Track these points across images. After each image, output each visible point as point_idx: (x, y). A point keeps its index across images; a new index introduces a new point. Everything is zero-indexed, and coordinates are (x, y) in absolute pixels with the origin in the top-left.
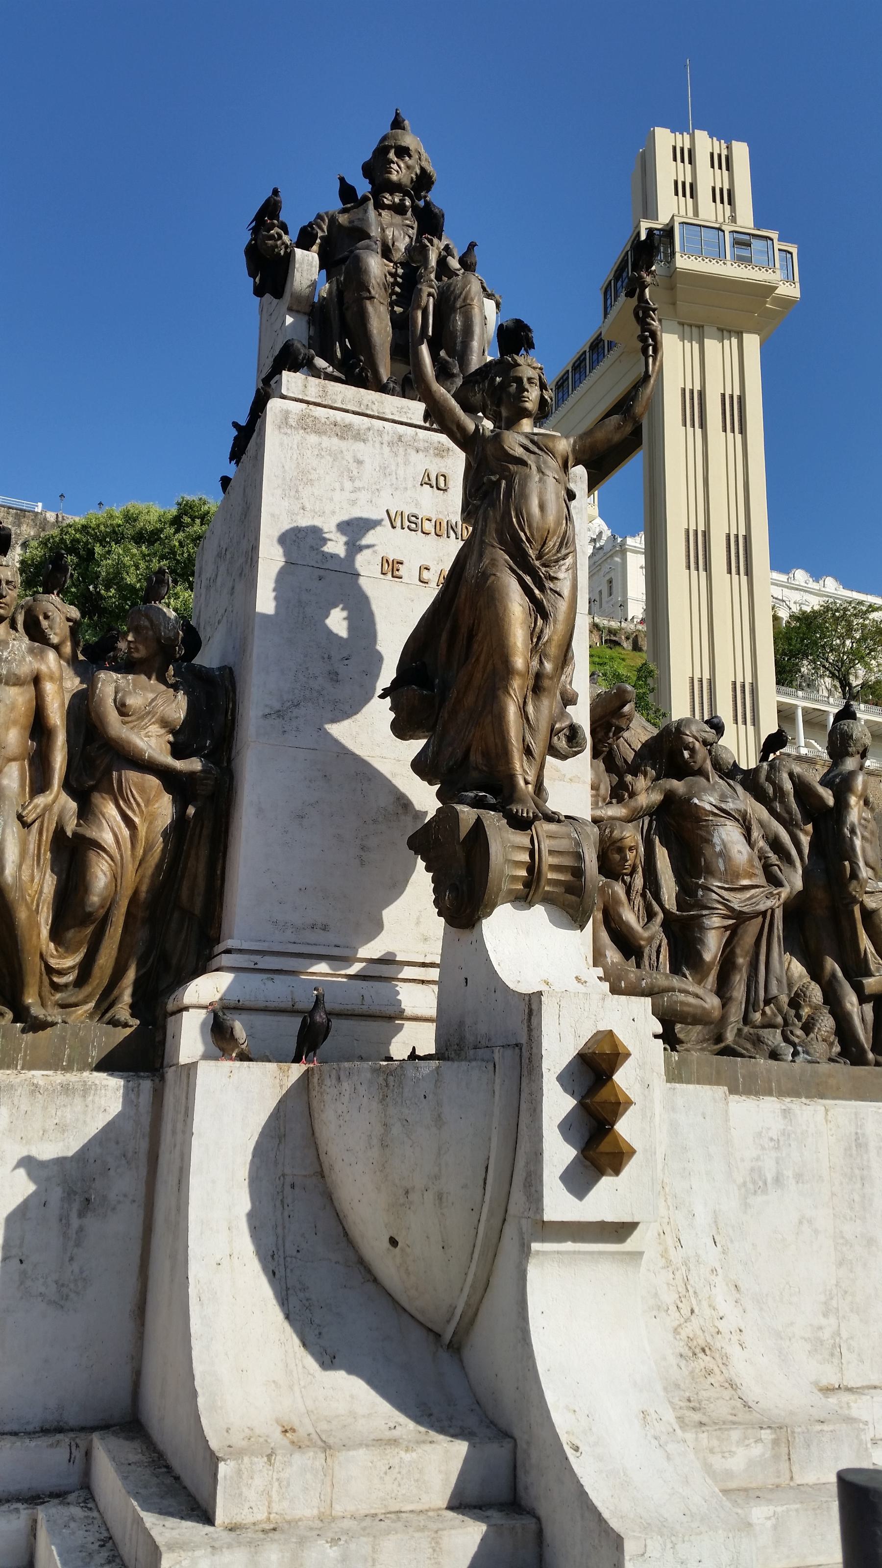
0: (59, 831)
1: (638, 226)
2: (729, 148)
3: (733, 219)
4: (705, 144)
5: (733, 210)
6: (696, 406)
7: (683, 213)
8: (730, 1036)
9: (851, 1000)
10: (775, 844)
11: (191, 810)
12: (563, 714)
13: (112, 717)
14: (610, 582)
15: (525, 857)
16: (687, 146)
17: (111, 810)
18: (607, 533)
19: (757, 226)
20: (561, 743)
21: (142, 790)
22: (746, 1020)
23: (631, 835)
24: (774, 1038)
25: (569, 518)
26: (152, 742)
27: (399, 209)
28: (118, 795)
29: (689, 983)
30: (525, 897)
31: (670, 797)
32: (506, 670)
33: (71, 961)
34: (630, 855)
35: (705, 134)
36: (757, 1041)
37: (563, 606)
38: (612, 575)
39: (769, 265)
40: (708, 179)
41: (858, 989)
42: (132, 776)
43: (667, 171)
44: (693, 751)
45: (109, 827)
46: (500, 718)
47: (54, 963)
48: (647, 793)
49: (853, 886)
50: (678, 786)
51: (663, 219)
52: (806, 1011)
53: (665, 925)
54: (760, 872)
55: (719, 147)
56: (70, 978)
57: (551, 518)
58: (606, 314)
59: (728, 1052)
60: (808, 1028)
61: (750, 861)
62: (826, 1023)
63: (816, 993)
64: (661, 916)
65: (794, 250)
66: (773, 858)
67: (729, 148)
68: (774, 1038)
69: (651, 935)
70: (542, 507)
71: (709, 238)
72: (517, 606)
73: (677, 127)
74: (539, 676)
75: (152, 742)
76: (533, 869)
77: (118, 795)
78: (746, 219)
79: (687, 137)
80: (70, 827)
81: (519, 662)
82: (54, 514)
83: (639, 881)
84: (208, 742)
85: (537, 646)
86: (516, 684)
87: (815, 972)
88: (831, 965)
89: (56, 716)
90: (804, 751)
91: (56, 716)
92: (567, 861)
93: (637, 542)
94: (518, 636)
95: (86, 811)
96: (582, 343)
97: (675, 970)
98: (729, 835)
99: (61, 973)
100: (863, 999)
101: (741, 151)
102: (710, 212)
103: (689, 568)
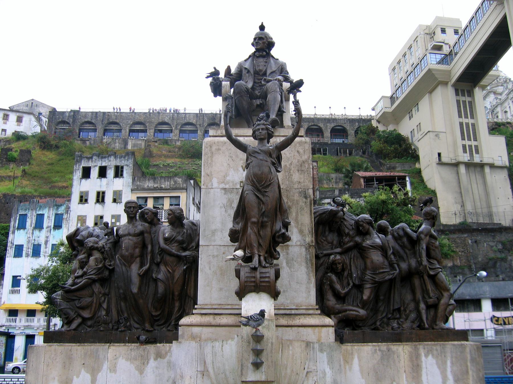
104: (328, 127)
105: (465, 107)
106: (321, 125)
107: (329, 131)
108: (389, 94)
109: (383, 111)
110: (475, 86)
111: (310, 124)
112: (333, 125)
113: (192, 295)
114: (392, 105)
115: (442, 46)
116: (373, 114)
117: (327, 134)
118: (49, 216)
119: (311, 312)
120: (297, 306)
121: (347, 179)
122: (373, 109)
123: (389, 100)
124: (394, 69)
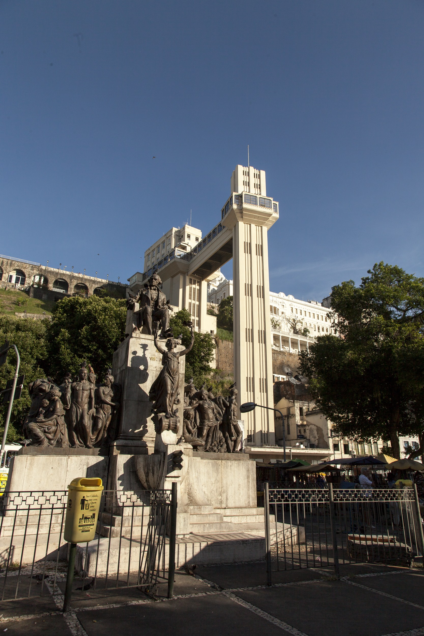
0: (93, 415)
1: (232, 194)
2: (260, 172)
3: (260, 194)
4: (252, 170)
5: (260, 191)
6: (248, 247)
7: (245, 191)
8: (208, 448)
9: (230, 442)
10: (219, 413)
11: (115, 412)
12: (177, 398)
13: (102, 395)
14: (224, 294)
15: (168, 423)
16: (247, 171)
17: (102, 412)
18: (224, 278)
19: (267, 196)
20: (176, 402)
21: (107, 408)
22: (211, 445)
23: (192, 413)
24: (215, 448)
25: (178, 368)
26: (108, 400)
27: (155, 290)
28: (103, 409)
29: (200, 439)
30: (168, 430)
31: (200, 404)
32: (167, 393)
33: (95, 437)
34: (191, 416)
35: (253, 168)
36: (212, 449)
37: (176, 383)
38: (225, 292)
39: (270, 207)
40: (253, 181)
41: (231, 439)
42: (106, 405)
43: (241, 178)
44: (204, 396)
45: (102, 415)
46: (166, 400)
47: (92, 438)
48: (196, 403)
49: (231, 421)
50: (201, 402)
51: (240, 192)
52: (222, 443)
53: (197, 428)
54: (214, 418)
55: (257, 172)
56: (94, 440)
57: (175, 367)
58: (222, 218)
59: (207, 451)
60: (221, 446)
61: (213, 417)
62: (225, 446)
63: (224, 440)
64: (196, 427)
65: (277, 203)
66: (218, 415)
67: (260, 172)
68: (215, 448)
69: (195, 430)
70: (174, 367)
71: (253, 200)
72: (169, 382)
73: (245, 165)
74: (172, 393)
75: (108, 400)
76: (169, 425)
77: (103, 409)
78: (264, 193)
79: (247, 168)
80: (95, 415)
81: (169, 392)
82: (45, 267)
83: (193, 420)
84: (131, 430)
85: (172, 389)
86: (168, 395)
87: (224, 435)
88: (227, 434)
89: (93, 395)
90: (282, 349)
91: (93, 395)
92: (175, 424)
93: (231, 282)
94: (169, 388)
95: (98, 412)
96: (215, 225)
97: (198, 437)
98: (210, 411)
99: (93, 439)
100: (232, 441)
101: (263, 173)
102: (253, 191)
103: (246, 295)
104: (93, 287)
105: (194, 293)
106: (87, 284)
107: (93, 290)
108: (143, 272)
109: (136, 283)
110: (203, 280)
111: (79, 282)
112: (96, 286)
113: (167, 475)
114: (143, 281)
115: (186, 247)
116: (129, 283)
117: (91, 292)
118: (130, 301)
119: (246, 511)
120: (105, 470)
121: (303, 331)
122: (129, 280)
123: (142, 276)
124: (148, 255)
